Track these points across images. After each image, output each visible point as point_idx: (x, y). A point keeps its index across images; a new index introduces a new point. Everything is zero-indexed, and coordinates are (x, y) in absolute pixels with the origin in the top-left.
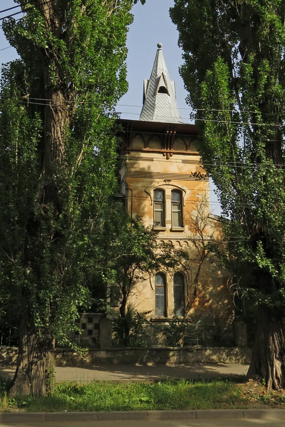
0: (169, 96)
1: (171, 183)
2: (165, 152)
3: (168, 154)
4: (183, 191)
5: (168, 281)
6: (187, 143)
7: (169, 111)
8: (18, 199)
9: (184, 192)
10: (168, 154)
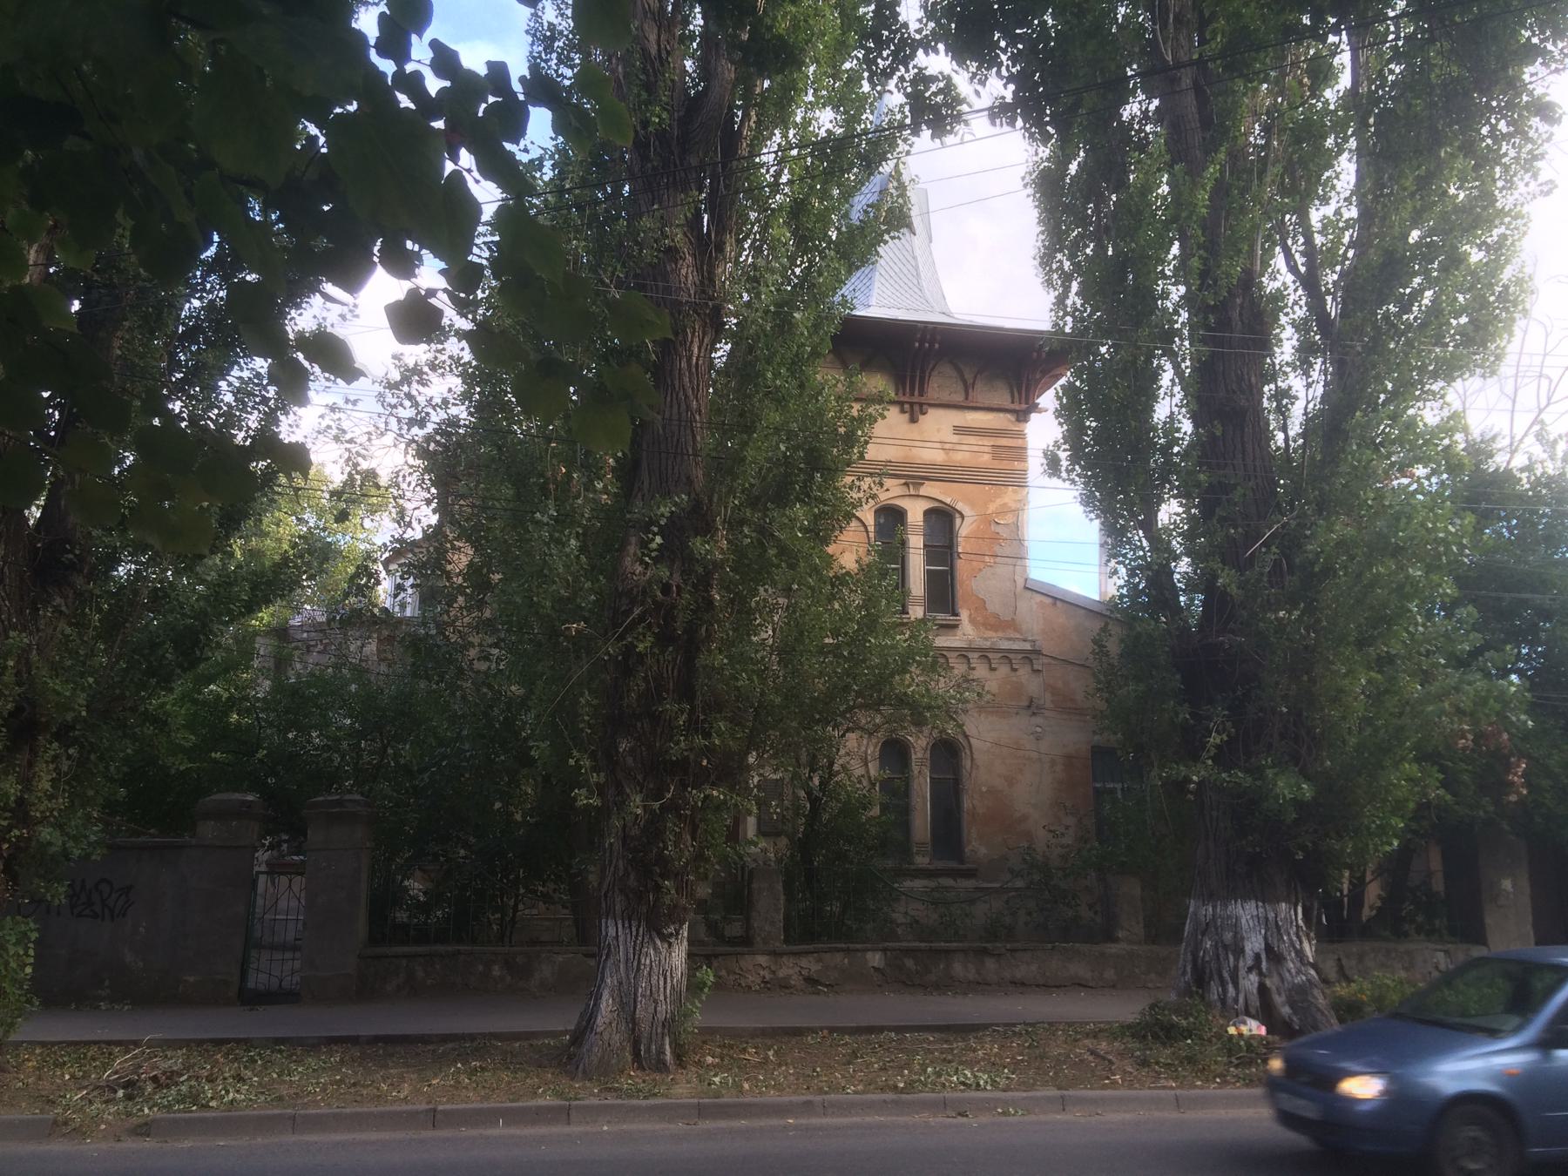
0: (915, 234)
1: (923, 491)
2: (907, 402)
3: (916, 408)
4: (957, 515)
5: (913, 764)
6: (969, 377)
7: (916, 282)
8: (1243, 578)
9: (957, 515)
10: (916, 408)
